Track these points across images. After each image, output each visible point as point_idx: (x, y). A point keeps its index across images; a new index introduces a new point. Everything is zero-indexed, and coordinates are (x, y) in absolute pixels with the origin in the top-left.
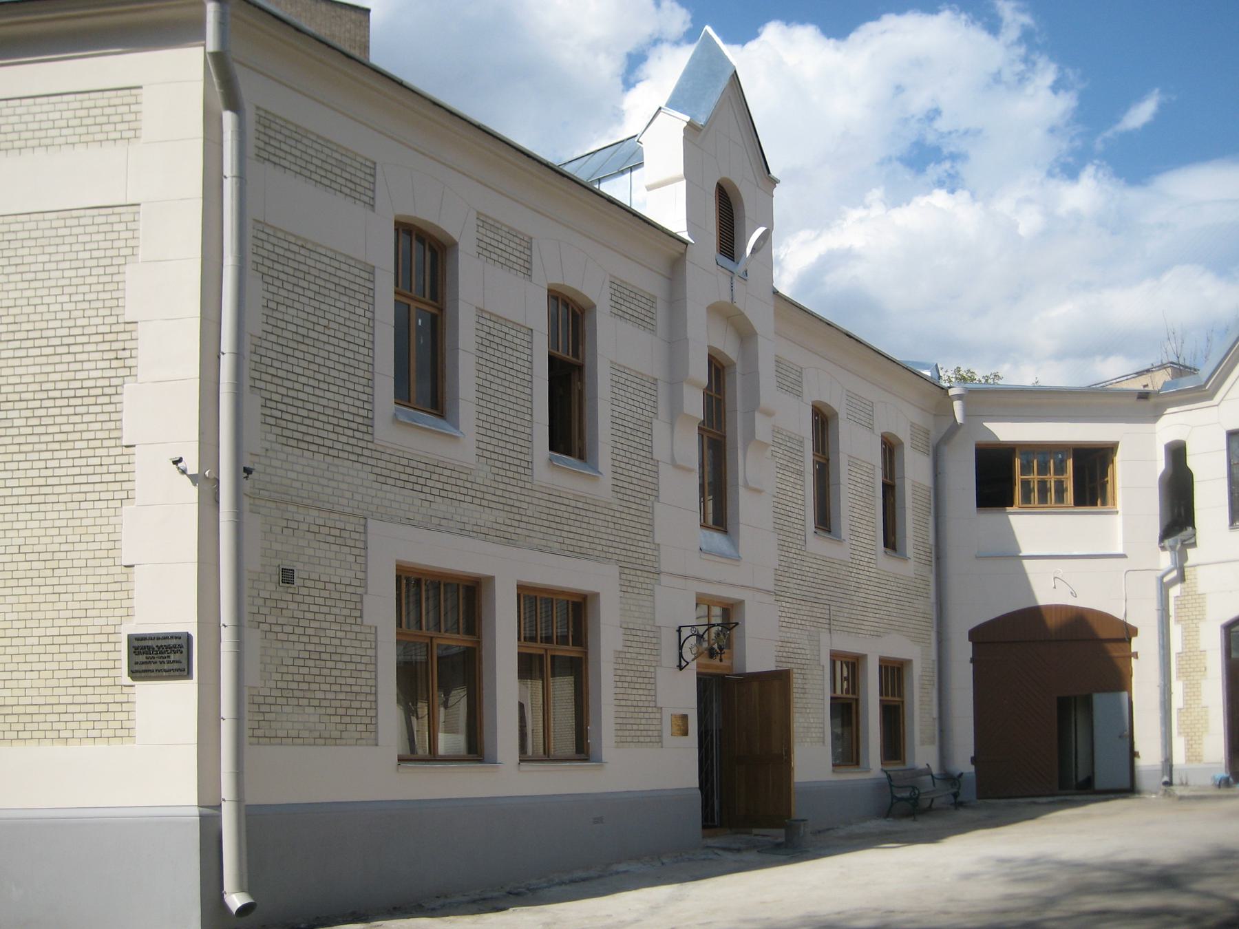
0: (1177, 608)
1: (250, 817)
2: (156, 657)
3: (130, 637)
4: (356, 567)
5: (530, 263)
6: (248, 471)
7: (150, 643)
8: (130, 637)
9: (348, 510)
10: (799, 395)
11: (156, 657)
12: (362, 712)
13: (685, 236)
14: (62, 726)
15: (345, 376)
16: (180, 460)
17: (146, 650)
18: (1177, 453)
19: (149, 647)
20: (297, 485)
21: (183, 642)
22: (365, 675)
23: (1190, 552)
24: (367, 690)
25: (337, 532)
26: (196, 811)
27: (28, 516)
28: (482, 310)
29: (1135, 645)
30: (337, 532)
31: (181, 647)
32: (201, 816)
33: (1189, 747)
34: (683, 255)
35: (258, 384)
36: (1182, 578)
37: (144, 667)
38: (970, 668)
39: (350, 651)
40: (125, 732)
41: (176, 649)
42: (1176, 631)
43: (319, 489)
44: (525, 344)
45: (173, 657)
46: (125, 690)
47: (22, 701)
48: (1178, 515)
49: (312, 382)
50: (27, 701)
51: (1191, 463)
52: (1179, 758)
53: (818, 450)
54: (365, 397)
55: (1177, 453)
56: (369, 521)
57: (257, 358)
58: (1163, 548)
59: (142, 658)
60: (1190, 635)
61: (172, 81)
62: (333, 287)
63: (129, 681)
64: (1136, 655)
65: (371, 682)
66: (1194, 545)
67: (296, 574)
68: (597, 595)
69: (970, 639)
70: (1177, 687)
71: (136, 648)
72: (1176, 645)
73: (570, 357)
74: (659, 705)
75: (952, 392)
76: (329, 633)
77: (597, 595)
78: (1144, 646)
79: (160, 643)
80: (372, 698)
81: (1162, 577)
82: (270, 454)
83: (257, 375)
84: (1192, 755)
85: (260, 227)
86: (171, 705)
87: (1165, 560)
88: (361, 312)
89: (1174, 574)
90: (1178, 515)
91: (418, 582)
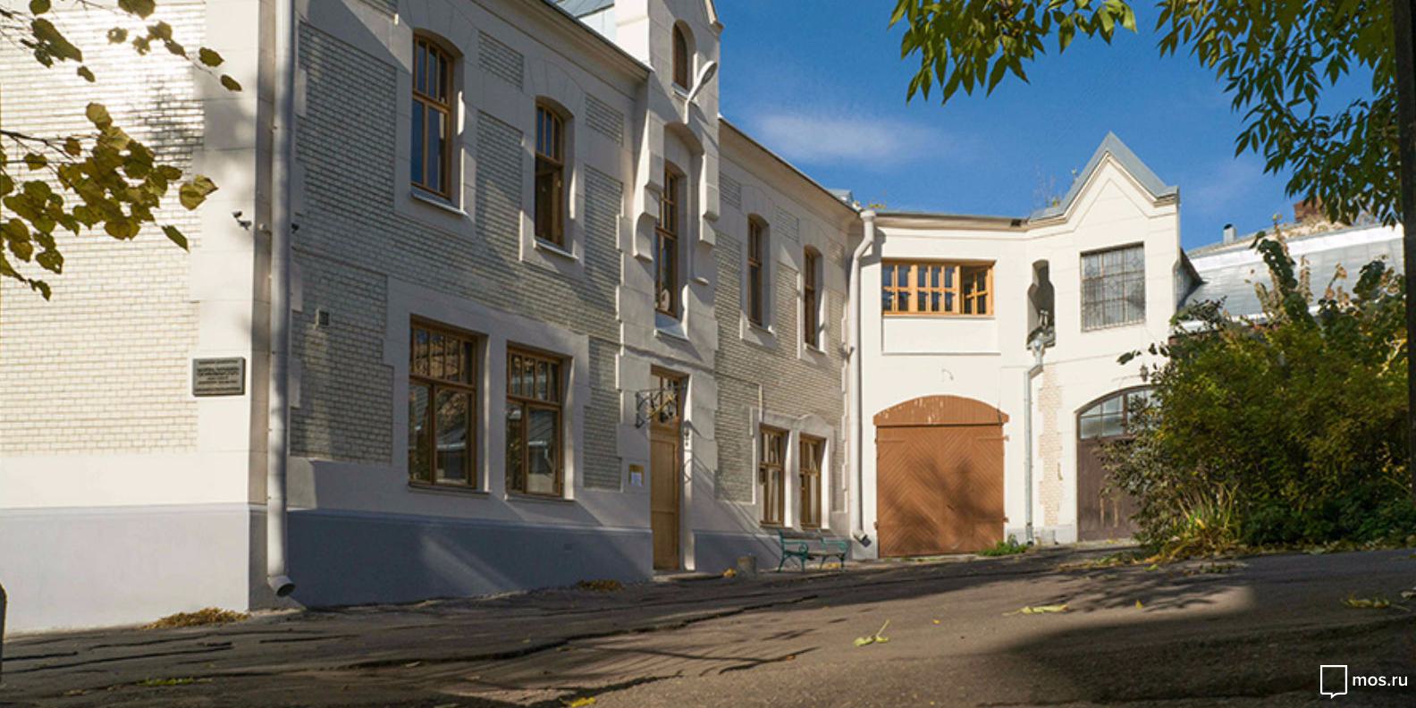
0: (1040, 398)
1: (291, 523)
2: (214, 378)
3: (196, 362)
4: (379, 316)
5: (522, 77)
6: (295, 227)
7: (213, 366)
8: (196, 362)
9: (374, 269)
10: (738, 207)
11: (214, 378)
12: (380, 438)
13: (648, 64)
14: (134, 437)
15: (372, 157)
16: (240, 214)
17: (209, 372)
18: (1042, 269)
19: (210, 369)
20: (333, 243)
21: (239, 365)
22: (384, 407)
24: (384, 419)
25: (363, 286)
26: (247, 509)
27: (109, 260)
28: (483, 113)
29: (1007, 429)
30: (363, 286)
31: (237, 369)
32: (251, 511)
33: (1048, 512)
34: (645, 80)
35: (303, 157)
37: (206, 386)
38: (874, 446)
39: (372, 385)
40: (188, 442)
41: (234, 371)
42: (1037, 417)
43: (348, 247)
44: (516, 166)
45: (230, 378)
46: (190, 406)
47: (102, 415)
49: (345, 159)
50: (107, 415)
51: (1053, 278)
53: (752, 255)
54: (387, 176)
55: (1042, 269)
56: (390, 279)
57: (301, 135)
59: (204, 379)
61: (1112, 135)
62: (362, 82)
63: (191, 397)
65: (388, 413)
67: (330, 317)
69: (875, 423)
70: (1038, 463)
71: (199, 370)
72: (1037, 430)
73: (552, 158)
74: (619, 455)
75: (863, 215)
76: (356, 369)
78: (1013, 430)
79: (220, 366)
80: (388, 426)
82: (312, 216)
83: (301, 149)
85: (305, 28)
86: (230, 418)
87: (1031, 360)
88: (385, 105)
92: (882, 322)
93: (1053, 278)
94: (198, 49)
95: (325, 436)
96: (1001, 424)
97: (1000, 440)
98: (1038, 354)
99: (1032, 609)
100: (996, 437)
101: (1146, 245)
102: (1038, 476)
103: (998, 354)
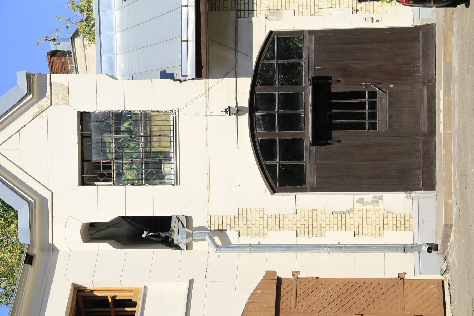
18: (93, 232)
23: (196, 223)
33: (395, 227)
36: (222, 232)
42: (274, 237)
48: (150, 232)
51: (106, 218)
52: (406, 238)
55: (93, 232)
58: (188, 247)
60: (278, 223)
64: (295, 274)
66: (188, 219)
68: (79, 185)
70: (332, 238)
72: (289, 238)
77: (79, 185)
78: (284, 266)
81: (217, 246)
84: (405, 224)
87: (202, 247)
89: (217, 239)
90: (150, 232)
91: (90, 235)
92: (187, 37)
93: (105, 217)
94: (137, 301)
95: (155, 128)
96: (279, 280)
97: (297, 280)
98: (196, 235)
99: (159, 234)
100: (294, 284)
101: (30, 72)
102: (346, 238)
103: (191, 283)
